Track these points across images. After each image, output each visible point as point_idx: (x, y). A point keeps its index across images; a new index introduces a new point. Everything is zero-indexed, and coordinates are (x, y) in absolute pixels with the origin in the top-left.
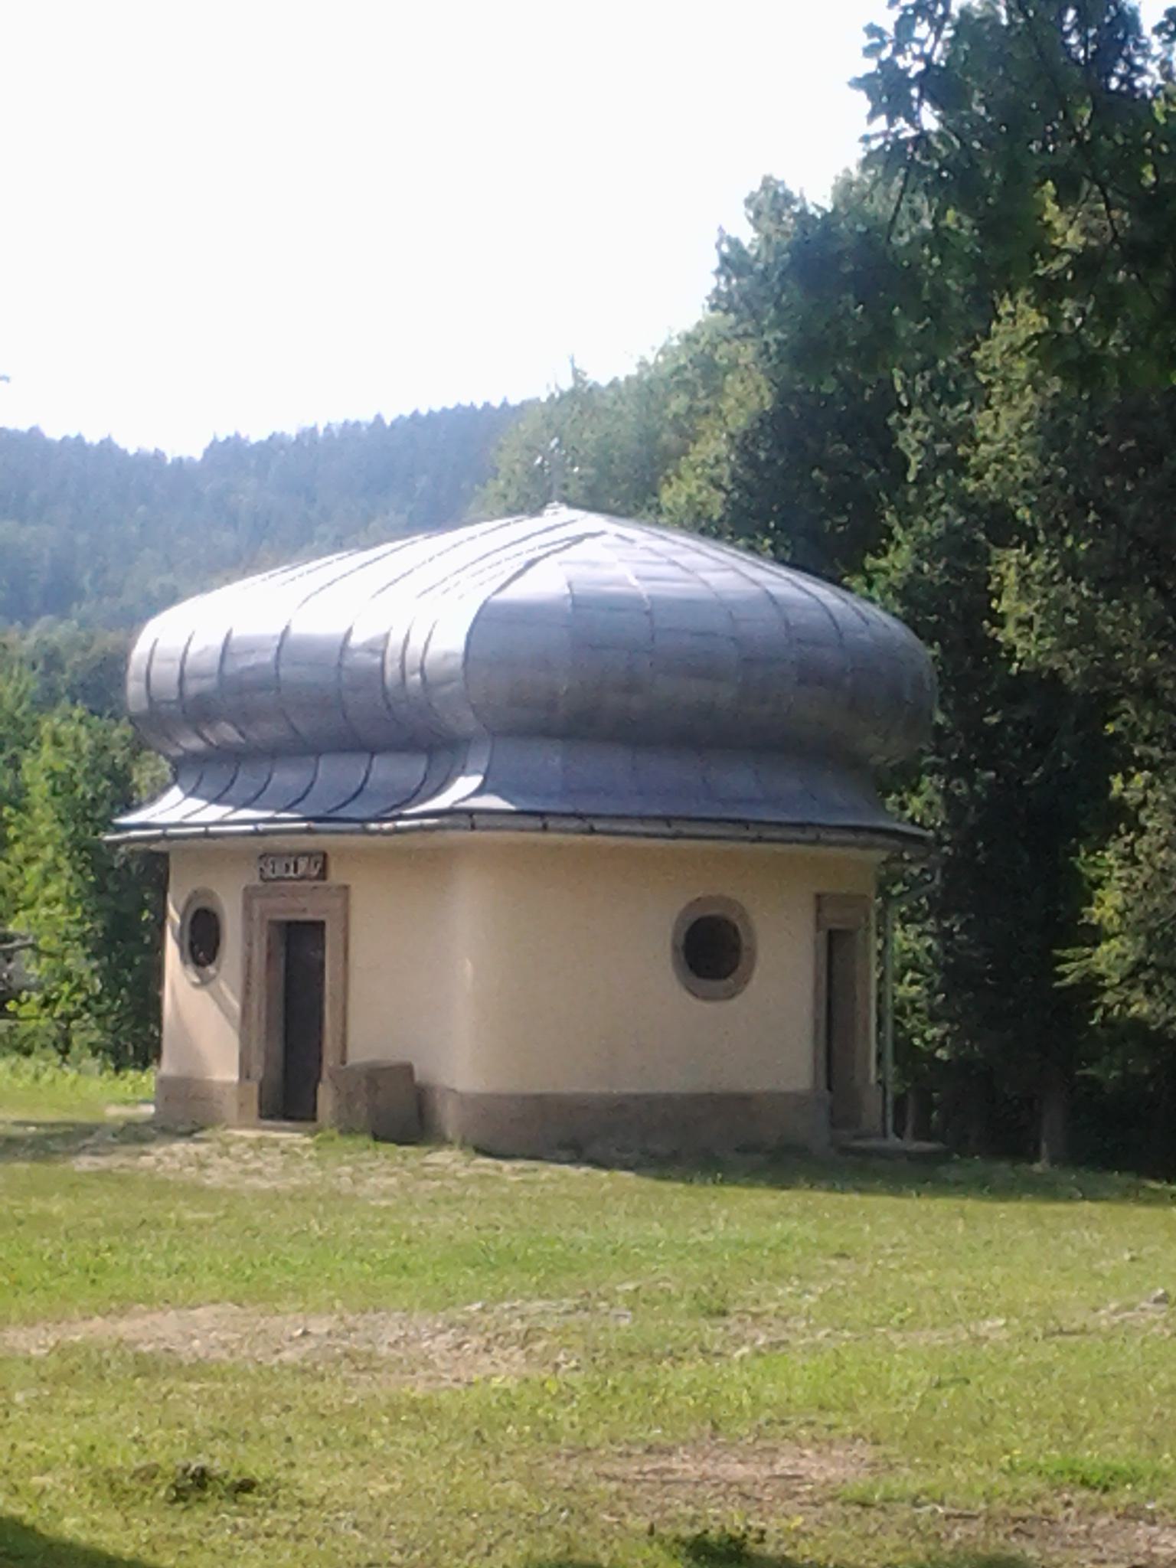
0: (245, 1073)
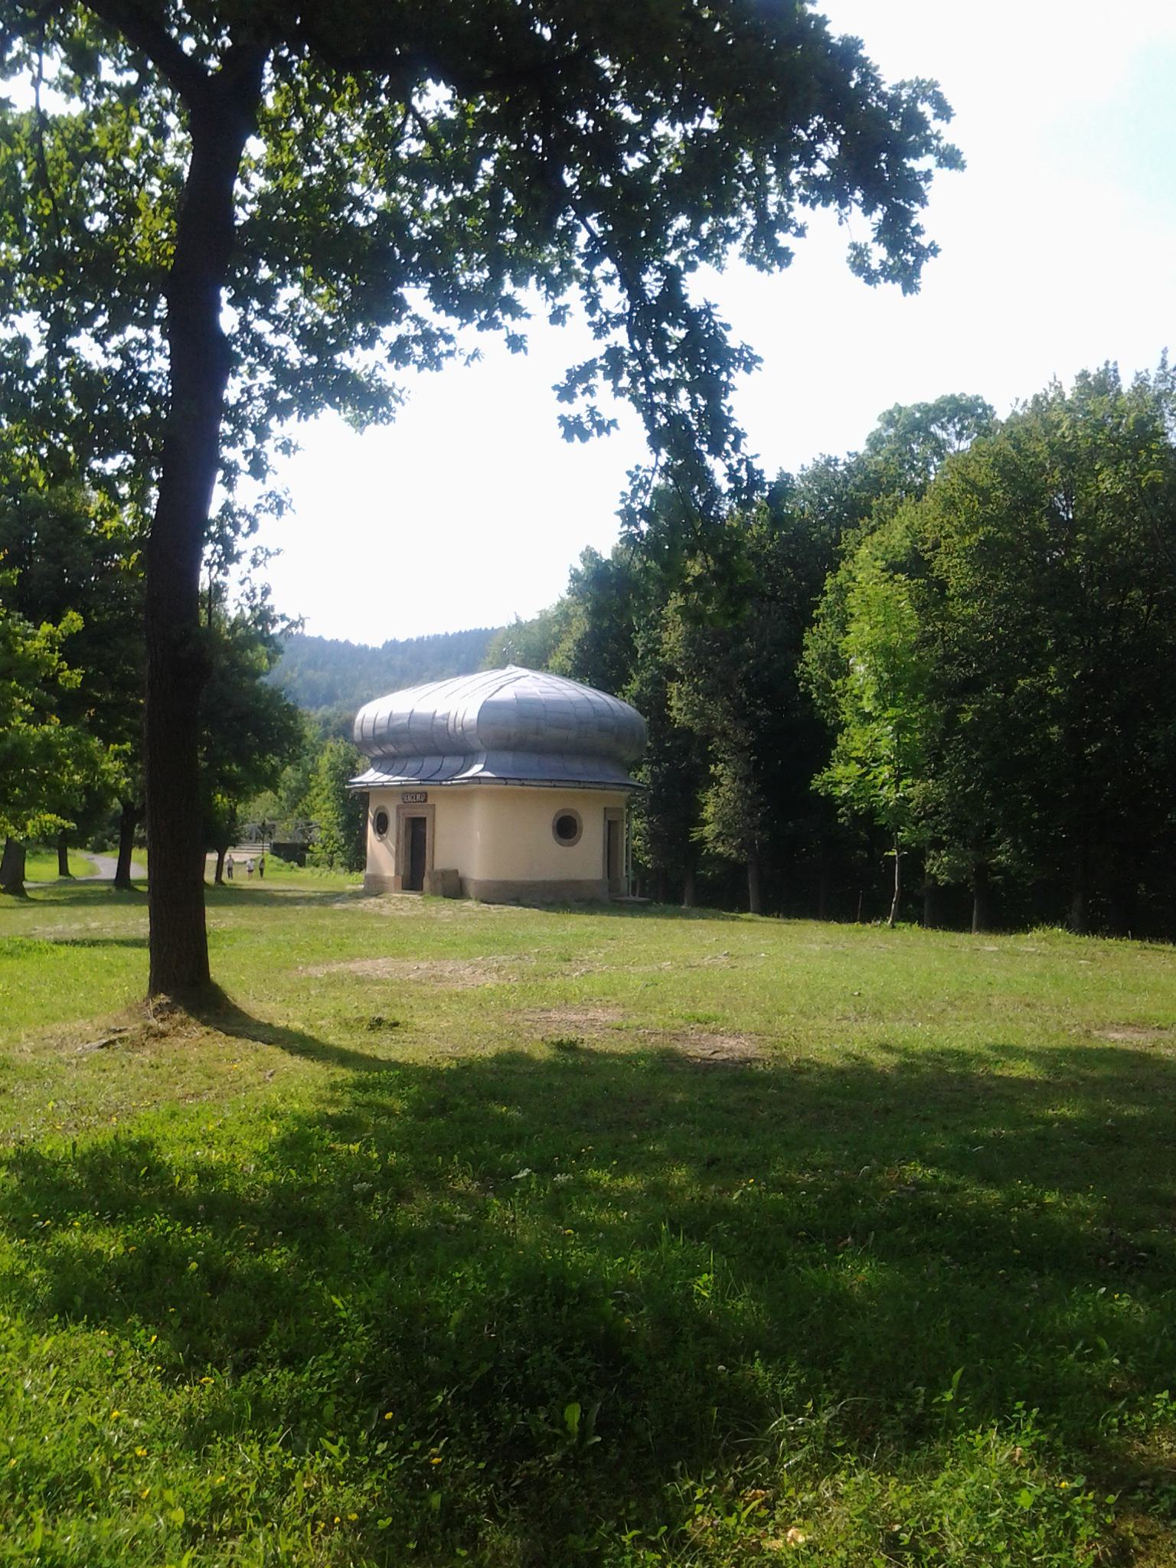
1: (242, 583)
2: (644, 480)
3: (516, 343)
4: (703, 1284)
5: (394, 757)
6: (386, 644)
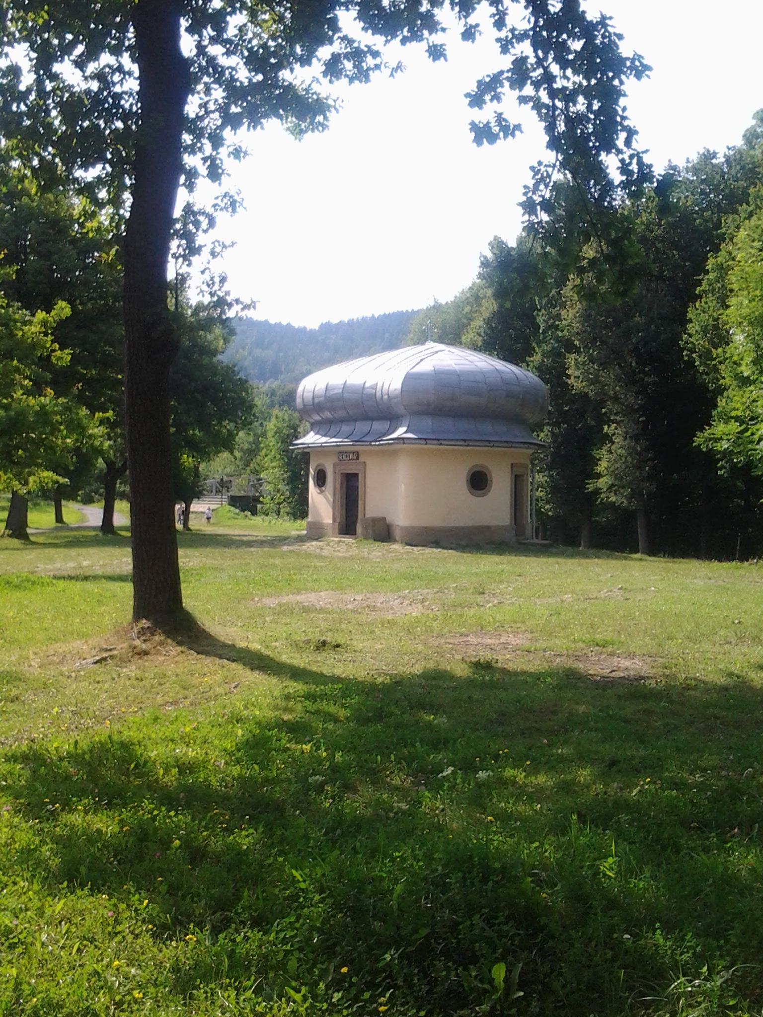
0: (334, 521)
1: (203, 272)
2: (545, 174)
3: (436, 52)
4: (608, 866)
5: (330, 422)
6: (322, 326)
